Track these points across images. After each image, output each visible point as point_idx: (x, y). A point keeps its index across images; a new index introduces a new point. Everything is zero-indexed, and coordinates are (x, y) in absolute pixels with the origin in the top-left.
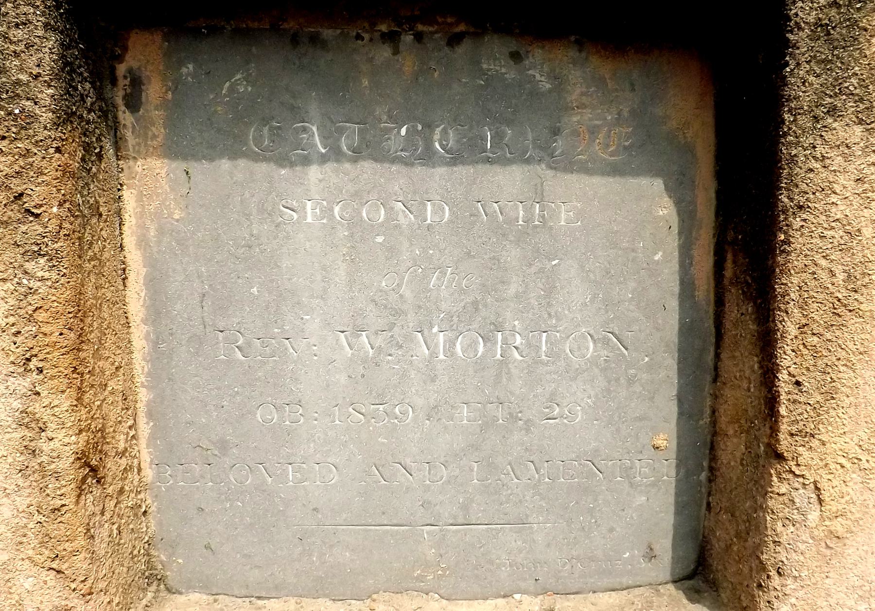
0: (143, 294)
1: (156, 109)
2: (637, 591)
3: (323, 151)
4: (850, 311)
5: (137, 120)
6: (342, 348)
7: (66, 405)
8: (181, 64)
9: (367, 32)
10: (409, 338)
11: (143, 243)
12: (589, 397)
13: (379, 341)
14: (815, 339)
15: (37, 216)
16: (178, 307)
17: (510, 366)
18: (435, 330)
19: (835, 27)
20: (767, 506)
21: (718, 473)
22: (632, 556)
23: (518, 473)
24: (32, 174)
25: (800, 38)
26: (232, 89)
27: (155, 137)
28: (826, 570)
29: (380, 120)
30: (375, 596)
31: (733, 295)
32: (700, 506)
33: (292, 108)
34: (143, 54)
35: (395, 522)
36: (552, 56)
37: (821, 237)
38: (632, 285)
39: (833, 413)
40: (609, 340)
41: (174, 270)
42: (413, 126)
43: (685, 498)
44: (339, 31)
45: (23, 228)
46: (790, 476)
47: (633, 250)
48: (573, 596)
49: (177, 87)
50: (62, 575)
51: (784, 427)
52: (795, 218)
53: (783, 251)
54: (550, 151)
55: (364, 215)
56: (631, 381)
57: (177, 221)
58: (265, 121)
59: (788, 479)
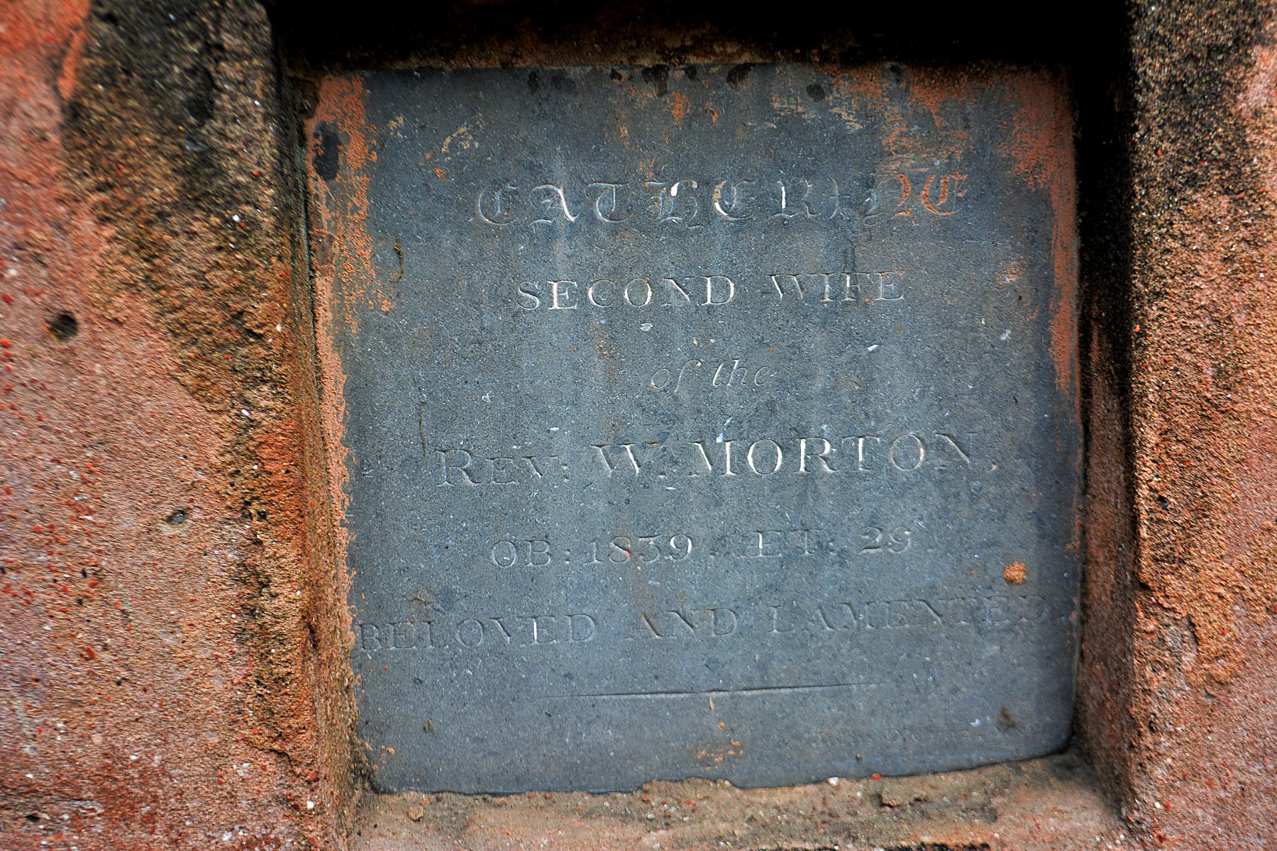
0: (342, 409)
1: (358, 172)
2: (990, 771)
3: (573, 219)
4: (1223, 412)
5: (333, 189)
6: (601, 467)
7: (292, 555)
8: (389, 117)
9: (625, 68)
10: (688, 452)
11: (342, 343)
12: (921, 519)
13: (648, 457)
14: (1181, 447)
15: (259, 337)
16: (388, 422)
17: (817, 482)
18: (719, 440)
19: (1193, 83)
20: (1134, 647)
21: (1089, 612)
22: (984, 724)
23: (831, 619)
24: (253, 288)
25: (1151, 101)
26: (453, 146)
27: (355, 209)
28: (1208, 723)
29: (644, 179)
30: (647, 787)
31: (1099, 385)
32: (1071, 656)
33: (531, 167)
34: (340, 102)
35: (672, 688)
36: (861, 89)
37: (1183, 328)
38: (972, 373)
39: (1206, 533)
40: (946, 444)
41: (383, 377)
42: (686, 184)
43: (1051, 646)
44: (589, 69)
45: (244, 351)
46: (1158, 610)
47: (972, 330)
48: (905, 779)
49: (383, 145)
50: (285, 758)
51: (1146, 552)
52: (1150, 307)
53: (1139, 345)
54: (862, 208)
55: (626, 296)
56: (974, 497)
57: (387, 313)
58: (497, 184)
59: (1156, 614)
